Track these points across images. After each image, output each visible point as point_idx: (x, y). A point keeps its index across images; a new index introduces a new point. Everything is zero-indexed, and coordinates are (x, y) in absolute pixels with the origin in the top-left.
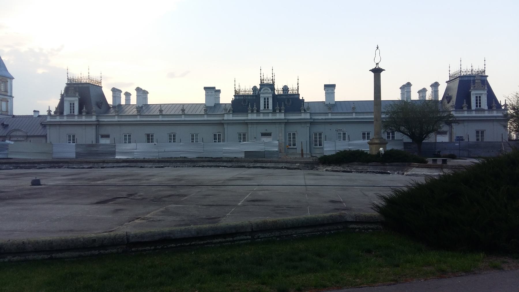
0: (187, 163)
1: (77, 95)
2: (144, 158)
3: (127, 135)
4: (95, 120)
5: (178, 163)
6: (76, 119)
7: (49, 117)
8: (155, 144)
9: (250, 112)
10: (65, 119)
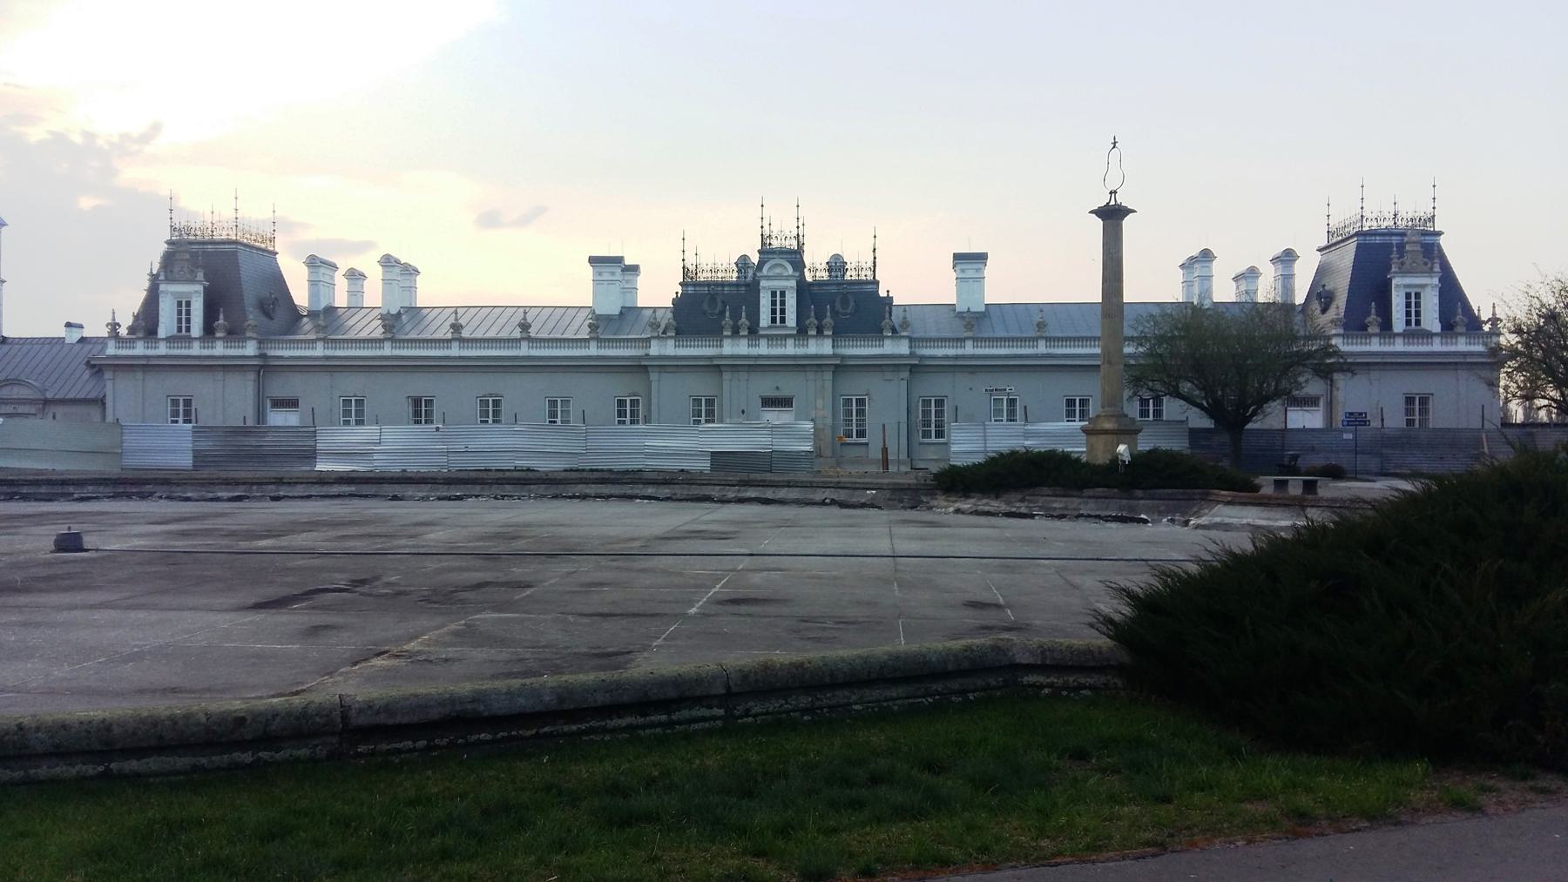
0: (536, 486)
1: (200, 275)
2: (404, 471)
4: (252, 354)
5: (508, 487)
6: (196, 350)
7: (111, 343)
8: (438, 429)
9: (729, 334)
10: (162, 350)
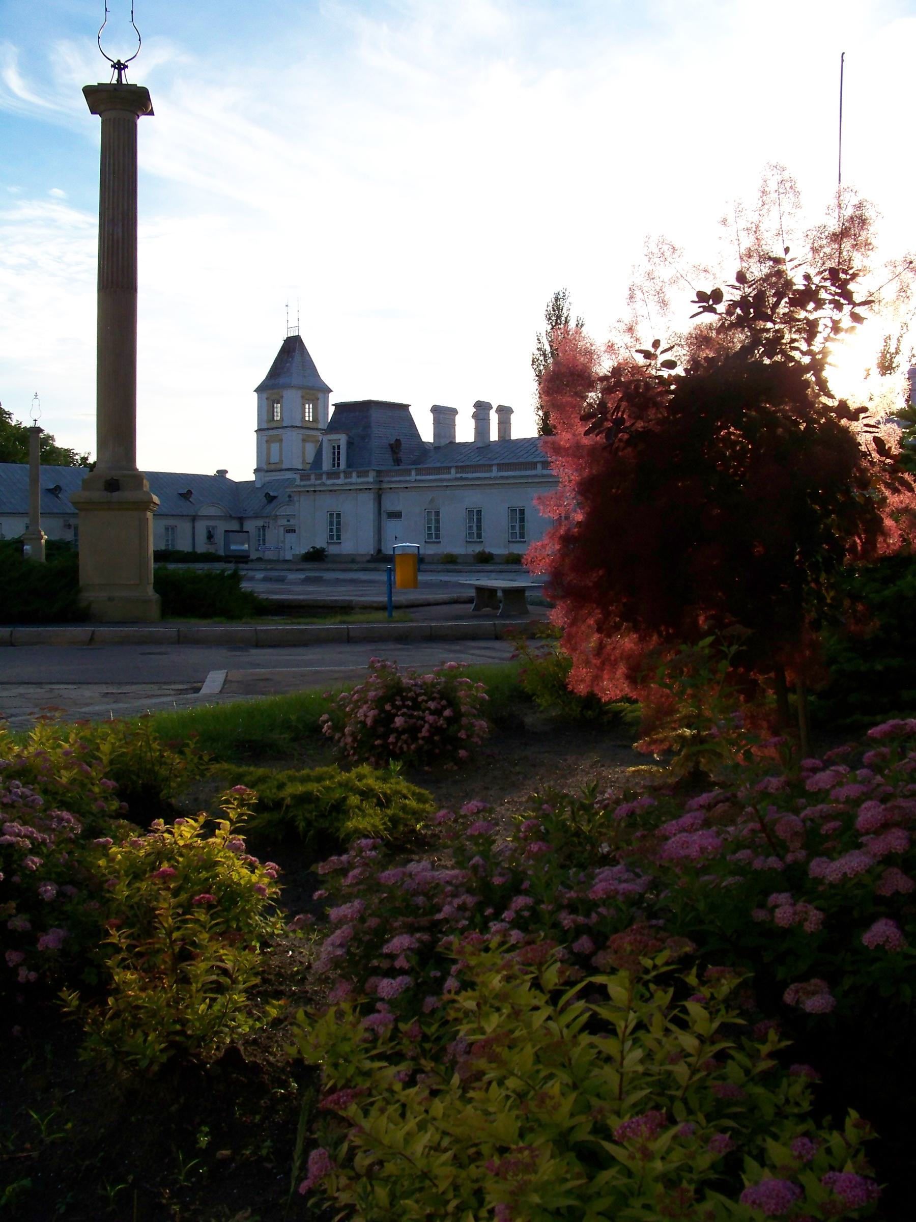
3: (475, 510)
